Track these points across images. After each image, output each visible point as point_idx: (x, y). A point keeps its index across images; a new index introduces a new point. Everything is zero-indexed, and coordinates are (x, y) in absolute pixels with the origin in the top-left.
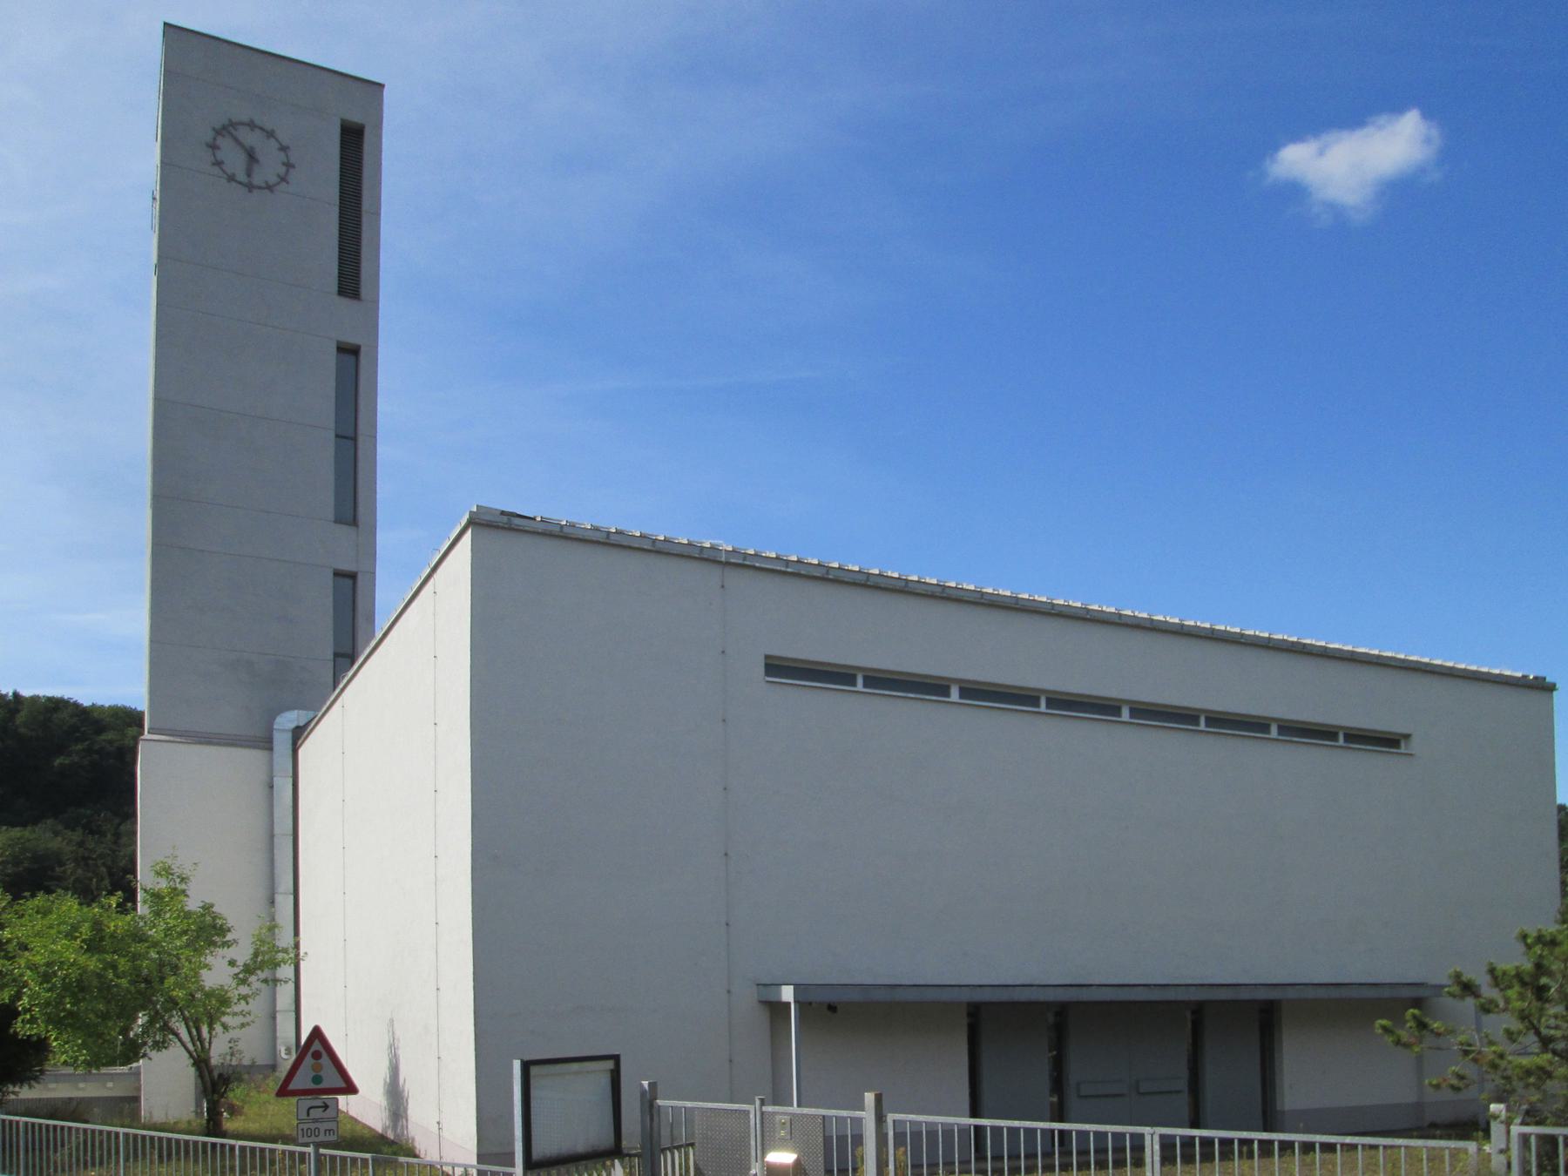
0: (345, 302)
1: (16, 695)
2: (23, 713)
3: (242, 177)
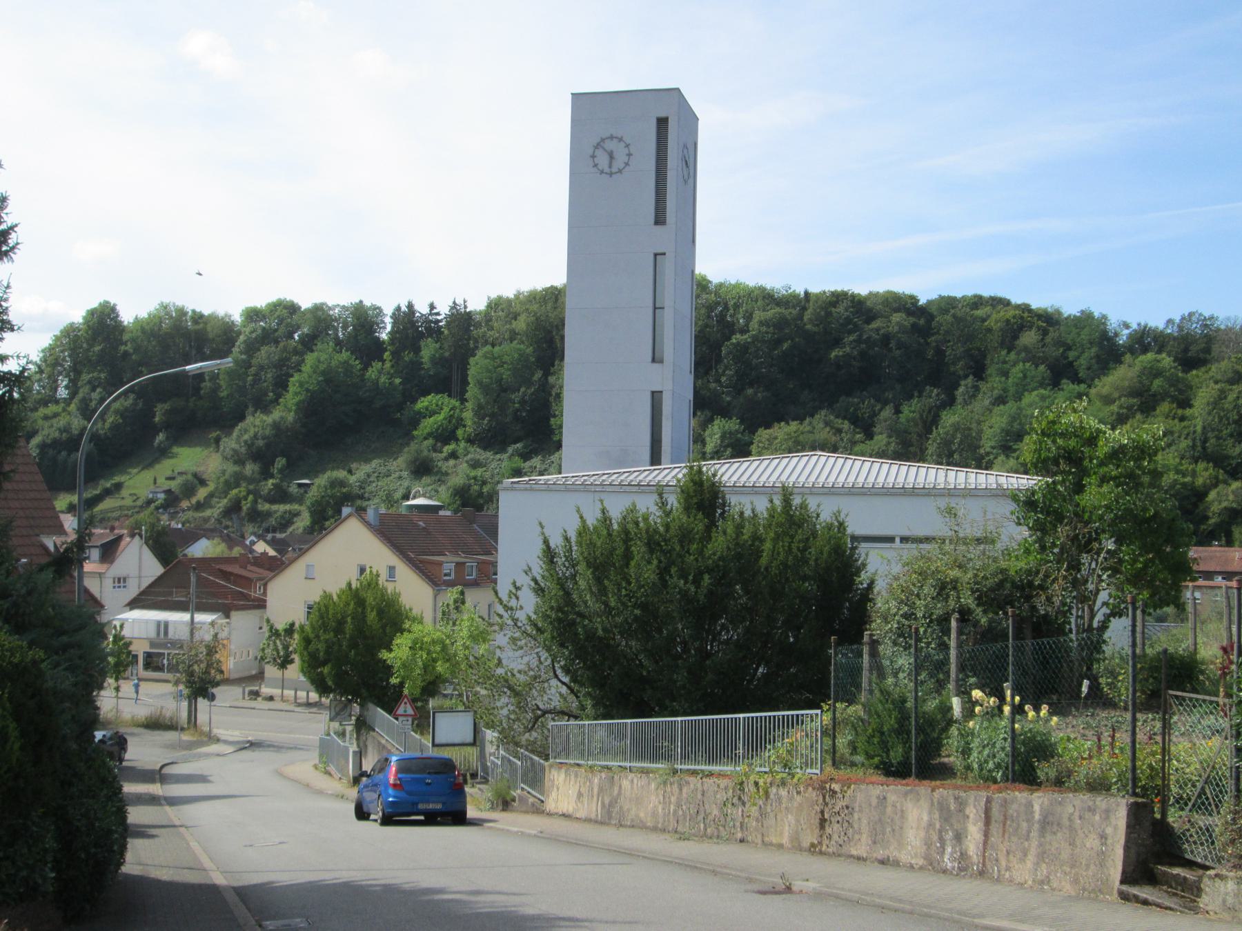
0: (659, 227)
1: (806, 293)
2: (809, 311)
3: (607, 170)
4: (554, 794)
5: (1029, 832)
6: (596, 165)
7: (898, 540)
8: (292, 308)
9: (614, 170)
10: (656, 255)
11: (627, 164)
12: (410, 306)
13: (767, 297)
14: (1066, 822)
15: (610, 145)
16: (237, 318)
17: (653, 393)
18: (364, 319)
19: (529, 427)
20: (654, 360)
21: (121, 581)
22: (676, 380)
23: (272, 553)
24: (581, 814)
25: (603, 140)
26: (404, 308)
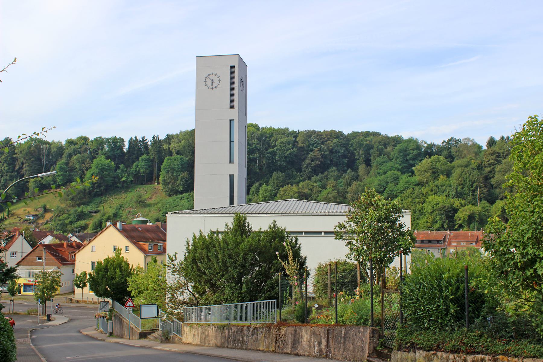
4: (185, 335)
5: (340, 340)
6: (206, 85)
7: (323, 233)
8: (86, 139)
9: (214, 87)
10: (230, 120)
11: (219, 84)
12: (136, 138)
13: (284, 132)
14: (351, 337)
15: (212, 77)
16: (64, 143)
17: (230, 175)
18: (116, 143)
19: (184, 186)
20: (230, 162)
21: (14, 254)
22: (238, 169)
23: (78, 241)
24: (195, 343)
25: (209, 75)
26: (134, 138)
